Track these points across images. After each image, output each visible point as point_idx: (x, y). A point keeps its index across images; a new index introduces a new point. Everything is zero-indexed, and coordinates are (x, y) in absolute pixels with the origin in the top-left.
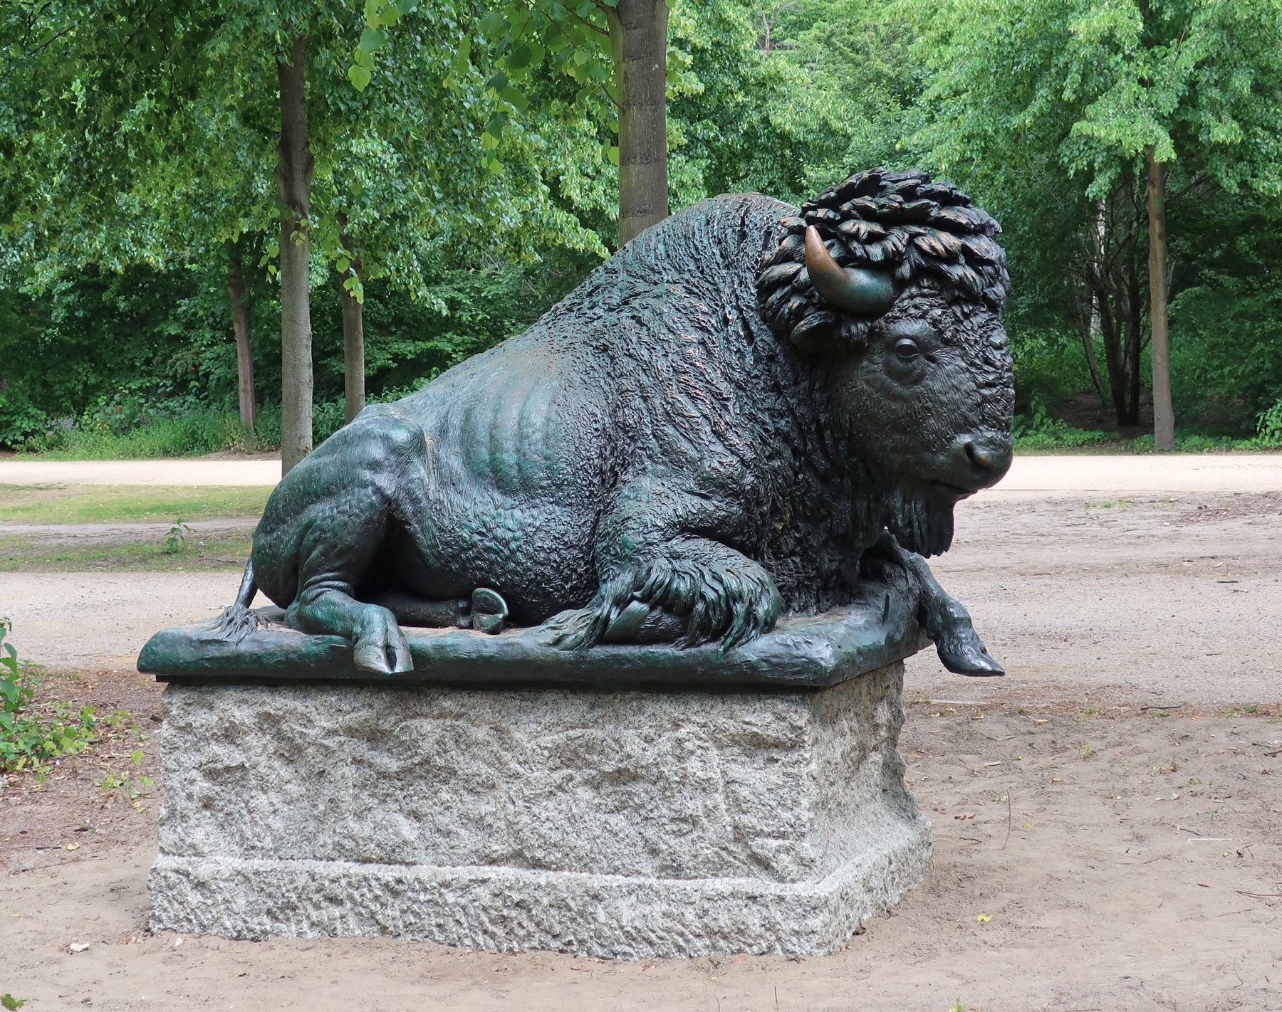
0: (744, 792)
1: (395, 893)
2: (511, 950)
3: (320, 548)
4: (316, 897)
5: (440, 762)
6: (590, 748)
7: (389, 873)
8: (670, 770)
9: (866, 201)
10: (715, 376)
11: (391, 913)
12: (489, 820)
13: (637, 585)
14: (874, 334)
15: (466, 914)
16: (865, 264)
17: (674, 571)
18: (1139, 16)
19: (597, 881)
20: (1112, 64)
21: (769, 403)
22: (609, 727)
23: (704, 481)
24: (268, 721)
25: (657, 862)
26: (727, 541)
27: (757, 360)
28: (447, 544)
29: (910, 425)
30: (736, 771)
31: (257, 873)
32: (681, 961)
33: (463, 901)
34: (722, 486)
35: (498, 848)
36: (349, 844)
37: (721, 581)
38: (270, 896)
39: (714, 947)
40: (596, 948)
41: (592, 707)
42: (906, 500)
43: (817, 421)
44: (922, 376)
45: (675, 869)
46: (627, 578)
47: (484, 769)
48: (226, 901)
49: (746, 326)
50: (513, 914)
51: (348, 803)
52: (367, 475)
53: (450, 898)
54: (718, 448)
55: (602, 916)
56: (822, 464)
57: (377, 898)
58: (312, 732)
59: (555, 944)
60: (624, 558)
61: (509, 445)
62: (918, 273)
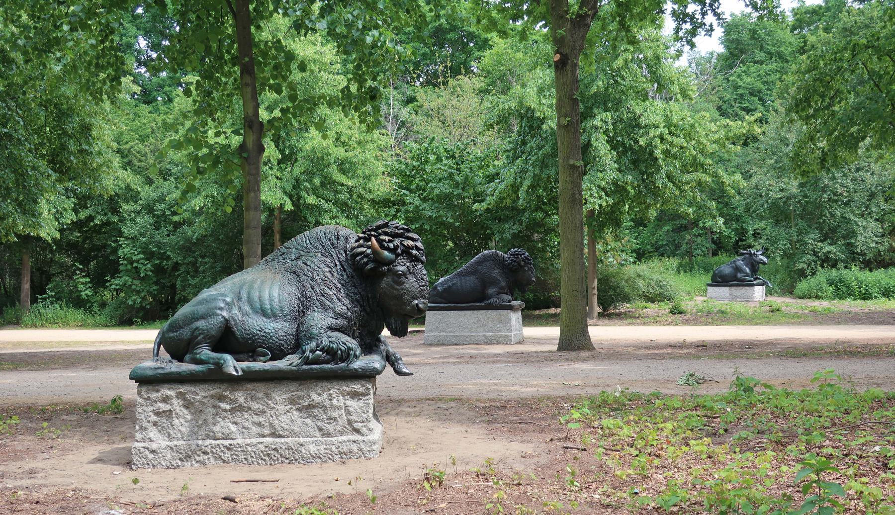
0: (351, 409)
1: (229, 449)
2: (271, 464)
3: (202, 336)
4: (198, 453)
5: (246, 405)
6: (299, 398)
7: (227, 443)
8: (327, 403)
9: (386, 230)
10: (336, 282)
11: (227, 455)
12: (263, 423)
13: (318, 346)
14: (389, 270)
15: (255, 454)
16: (388, 249)
17: (330, 342)
18: (277, 152)
19: (301, 440)
20: (265, 170)
21: (353, 291)
22: (305, 391)
23: (336, 314)
24: (180, 395)
25: (321, 433)
26: (343, 332)
27: (348, 277)
28: (248, 334)
29: (399, 298)
30: (348, 403)
31: (176, 446)
32: (330, 463)
33: (254, 450)
34: (342, 316)
35: (267, 432)
36: (212, 434)
37: (345, 344)
38: (181, 453)
39: (342, 458)
40: (301, 461)
41: (300, 386)
42: (395, 320)
43: (368, 297)
44: (404, 283)
45: (329, 435)
46: (314, 344)
47: (261, 407)
48: (163, 456)
49: (342, 266)
50: (272, 452)
51: (210, 420)
52: (219, 312)
53: (250, 449)
54: (340, 304)
55: (304, 451)
56: (368, 310)
57: (222, 451)
58: (198, 397)
59: (288, 461)
60: (311, 338)
61: (267, 303)
62: (403, 252)
